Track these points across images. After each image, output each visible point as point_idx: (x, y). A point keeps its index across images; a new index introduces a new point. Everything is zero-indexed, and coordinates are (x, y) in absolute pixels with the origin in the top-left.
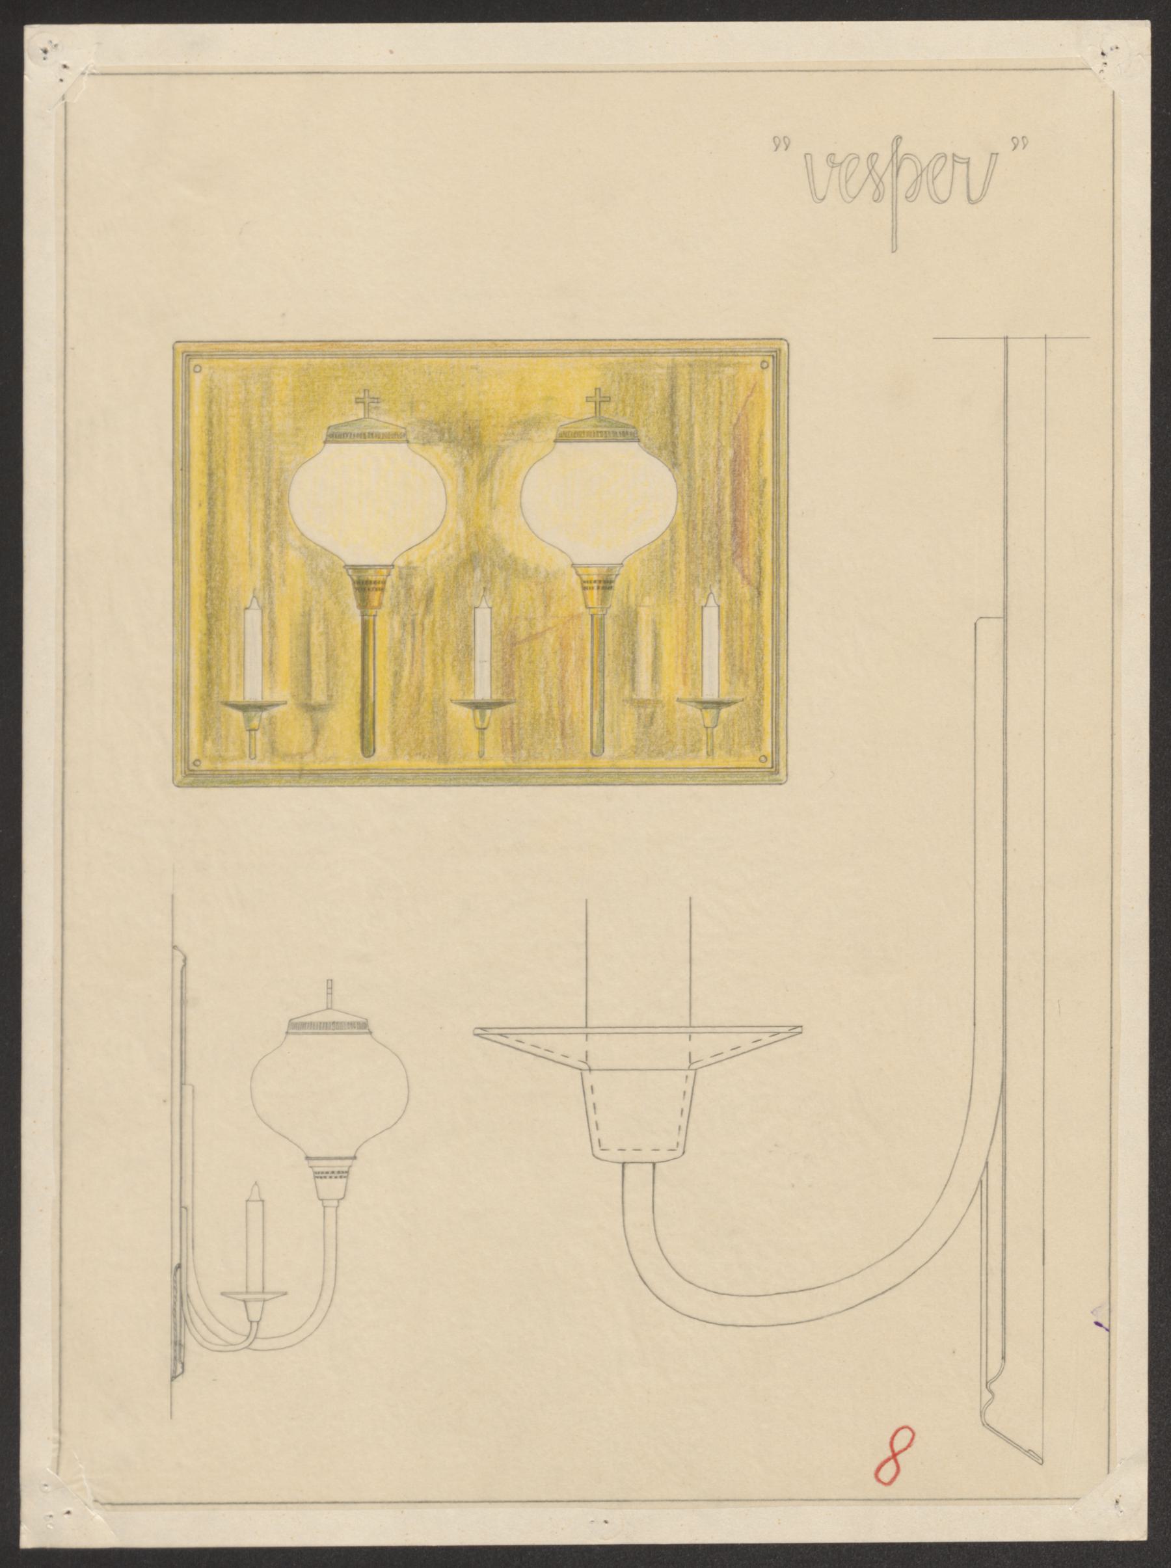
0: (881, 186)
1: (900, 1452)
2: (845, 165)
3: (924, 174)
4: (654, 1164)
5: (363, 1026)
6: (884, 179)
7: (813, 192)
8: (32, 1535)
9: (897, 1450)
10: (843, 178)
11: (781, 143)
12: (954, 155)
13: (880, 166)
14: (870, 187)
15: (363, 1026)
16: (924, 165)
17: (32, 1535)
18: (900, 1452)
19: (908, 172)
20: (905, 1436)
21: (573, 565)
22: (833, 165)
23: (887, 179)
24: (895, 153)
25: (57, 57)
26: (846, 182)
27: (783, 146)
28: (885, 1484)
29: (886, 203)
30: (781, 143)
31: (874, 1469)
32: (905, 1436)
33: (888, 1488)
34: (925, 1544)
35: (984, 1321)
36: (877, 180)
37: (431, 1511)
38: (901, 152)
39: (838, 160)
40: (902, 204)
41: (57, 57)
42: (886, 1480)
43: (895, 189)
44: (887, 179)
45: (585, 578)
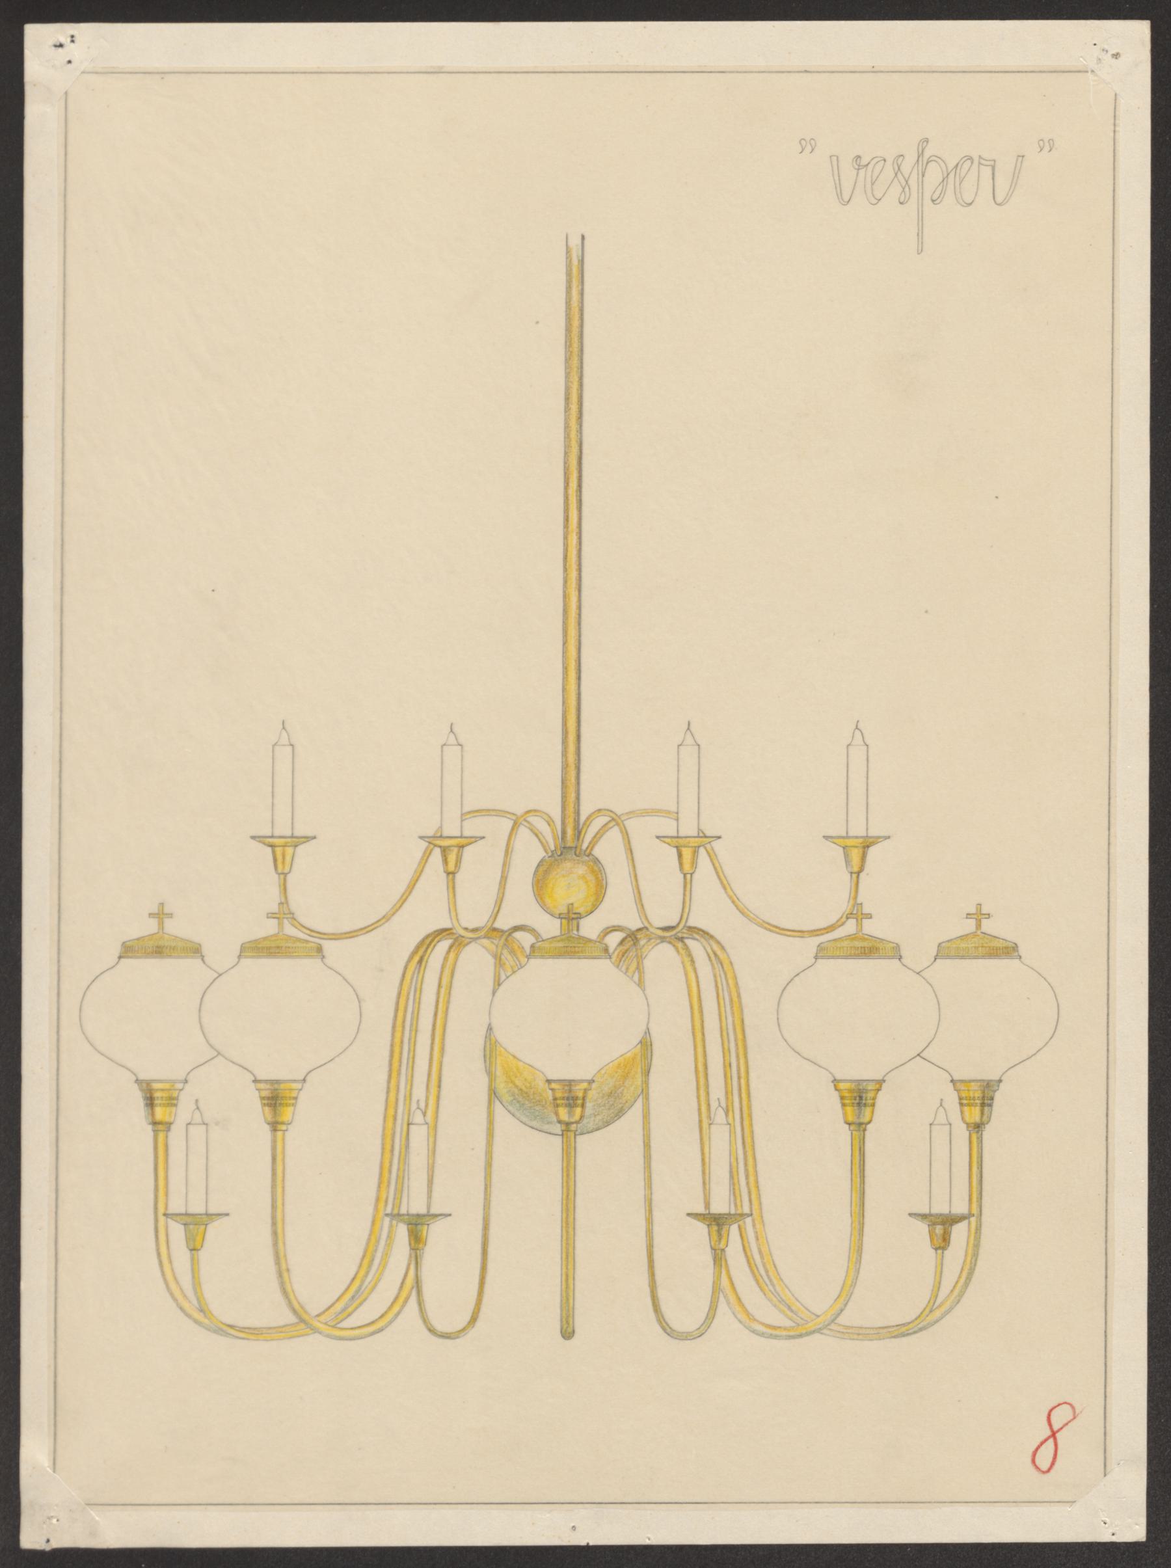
0: (907, 189)
2: (870, 166)
3: (952, 175)
6: (910, 182)
7: (840, 195)
8: (33, 1536)
10: (869, 180)
13: (906, 168)
14: (896, 190)
17: (33, 1536)
19: (934, 174)
20: (1044, 1459)
21: (952, 1081)
24: (920, 154)
25: (55, 55)
26: (873, 184)
29: (913, 204)
31: (1029, 1460)
32: (1044, 1459)
34: (1150, 993)
35: (700, 1050)
36: (904, 183)
38: (927, 154)
39: (864, 161)
41: (55, 55)
42: (1045, 1467)
44: (913, 182)
45: (963, 1095)
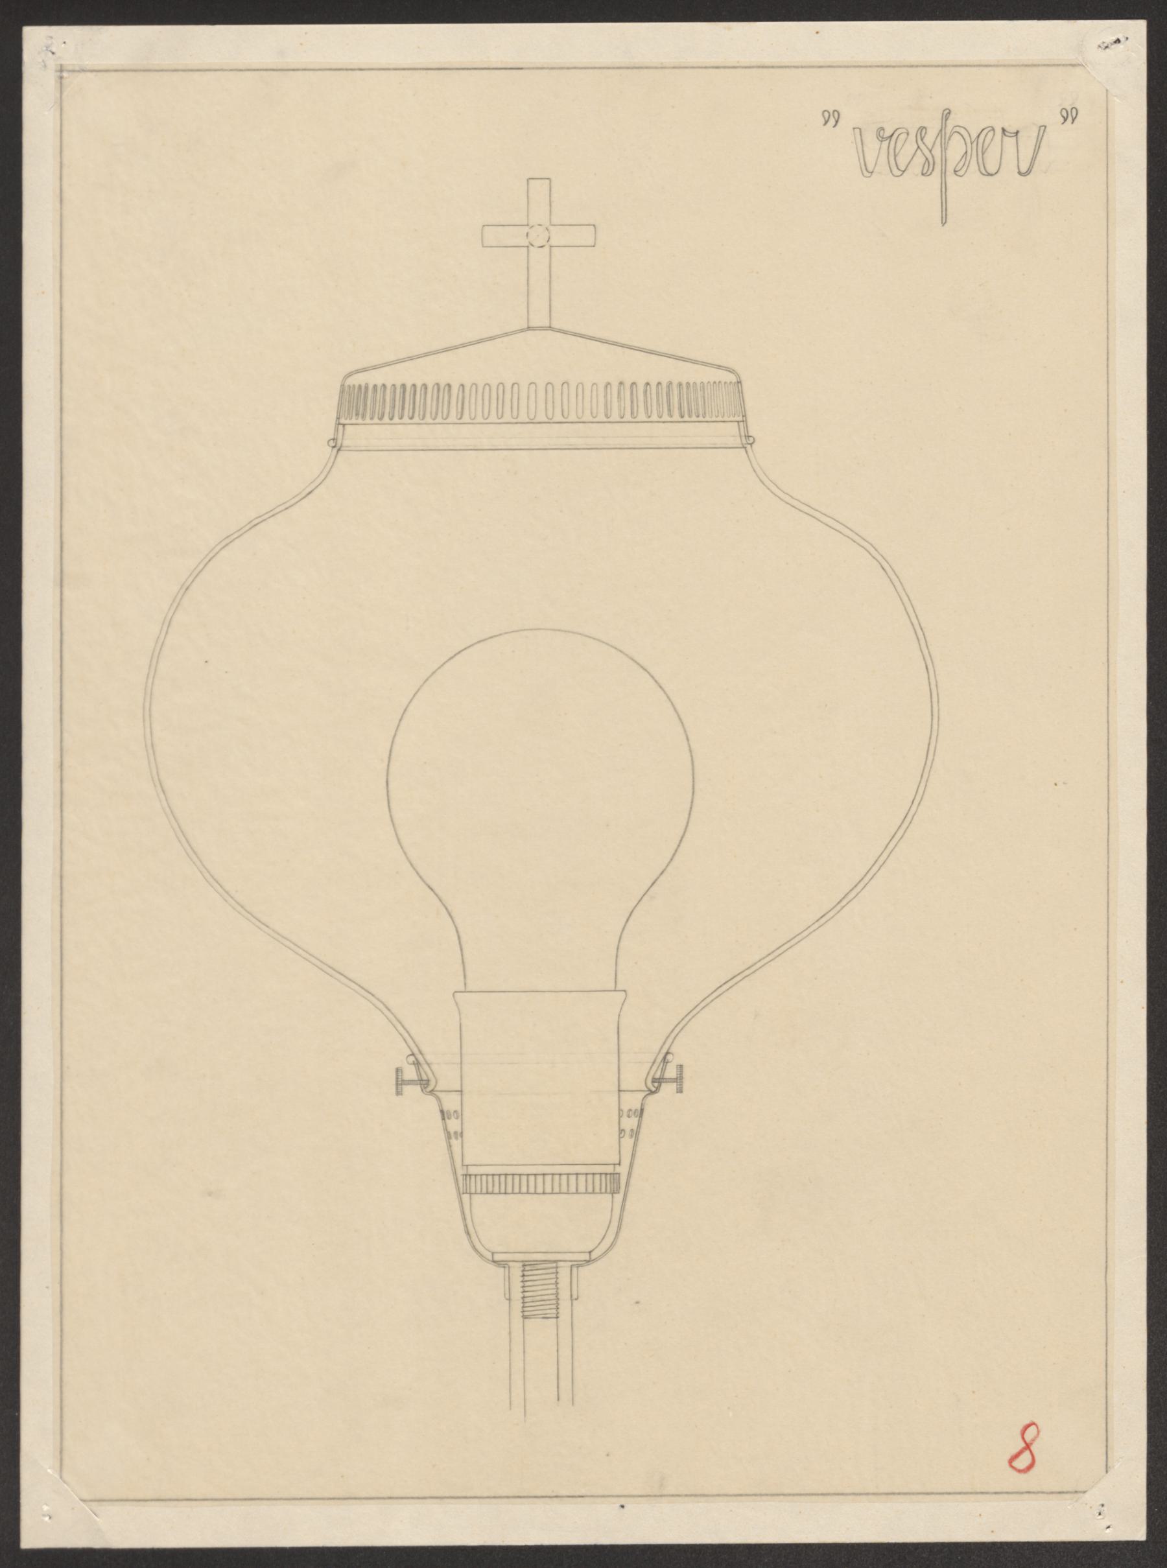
1: (1033, 1440)
4: (613, 1182)
5: (703, 402)
8: (44, 47)
9: (1028, 1440)
11: (832, 117)
12: (1004, 130)
14: (919, 160)
15: (703, 402)
16: (974, 136)
17: (44, 47)
18: (1033, 1440)
19: (956, 148)
22: (882, 139)
23: (937, 152)
27: (832, 122)
28: (1019, 1471)
29: (936, 177)
30: (832, 117)
33: (1023, 1476)
37: (561, 1360)
39: (887, 134)
40: (951, 179)
43: (945, 161)
44: (937, 152)
